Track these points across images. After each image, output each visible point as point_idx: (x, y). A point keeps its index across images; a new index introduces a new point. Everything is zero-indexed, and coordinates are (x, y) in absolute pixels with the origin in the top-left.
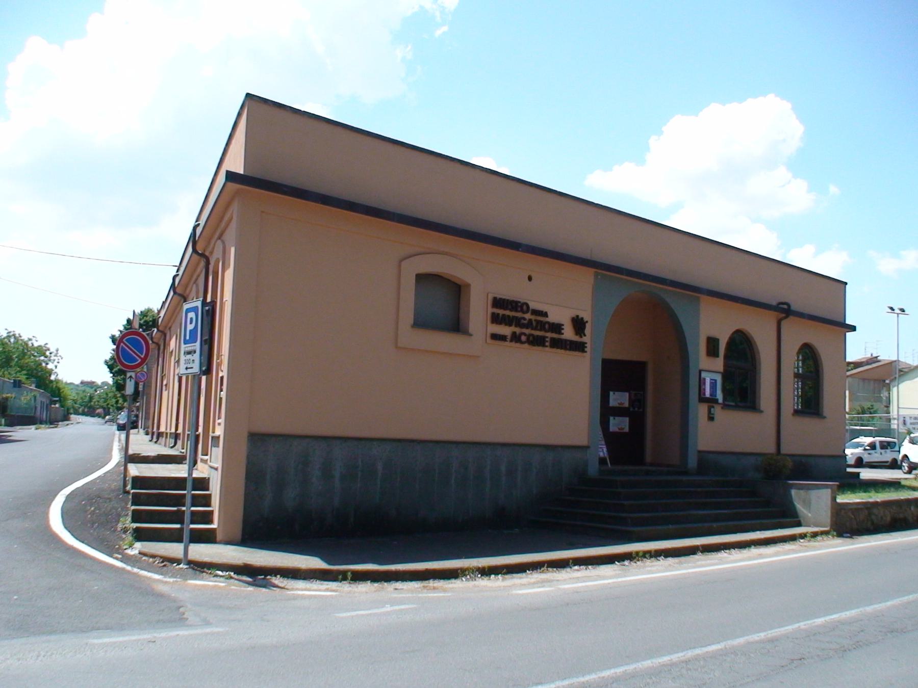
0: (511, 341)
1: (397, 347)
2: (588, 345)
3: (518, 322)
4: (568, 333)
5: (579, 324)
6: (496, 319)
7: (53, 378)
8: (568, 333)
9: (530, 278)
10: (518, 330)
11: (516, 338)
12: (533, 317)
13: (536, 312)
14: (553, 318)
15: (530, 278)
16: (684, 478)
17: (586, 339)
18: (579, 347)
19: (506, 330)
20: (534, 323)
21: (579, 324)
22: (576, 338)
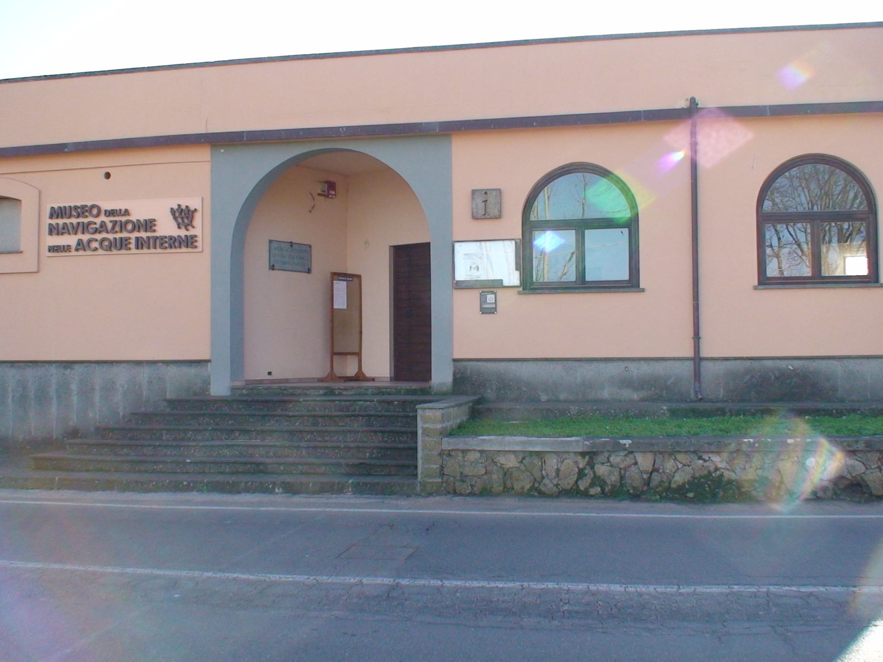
0: (77, 250)
1: (38, 272)
2: (199, 239)
3: (85, 228)
4: (167, 227)
5: (183, 216)
6: (53, 230)
7: (469, 371)
8: (167, 227)
9: (108, 175)
10: (85, 237)
11: (80, 245)
12: (107, 220)
13: (111, 213)
14: (139, 214)
15: (108, 175)
16: (288, 385)
17: (196, 231)
18: (189, 242)
19: (70, 240)
20: (110, 226)
21: (183, 216)
22: (183, 233)
